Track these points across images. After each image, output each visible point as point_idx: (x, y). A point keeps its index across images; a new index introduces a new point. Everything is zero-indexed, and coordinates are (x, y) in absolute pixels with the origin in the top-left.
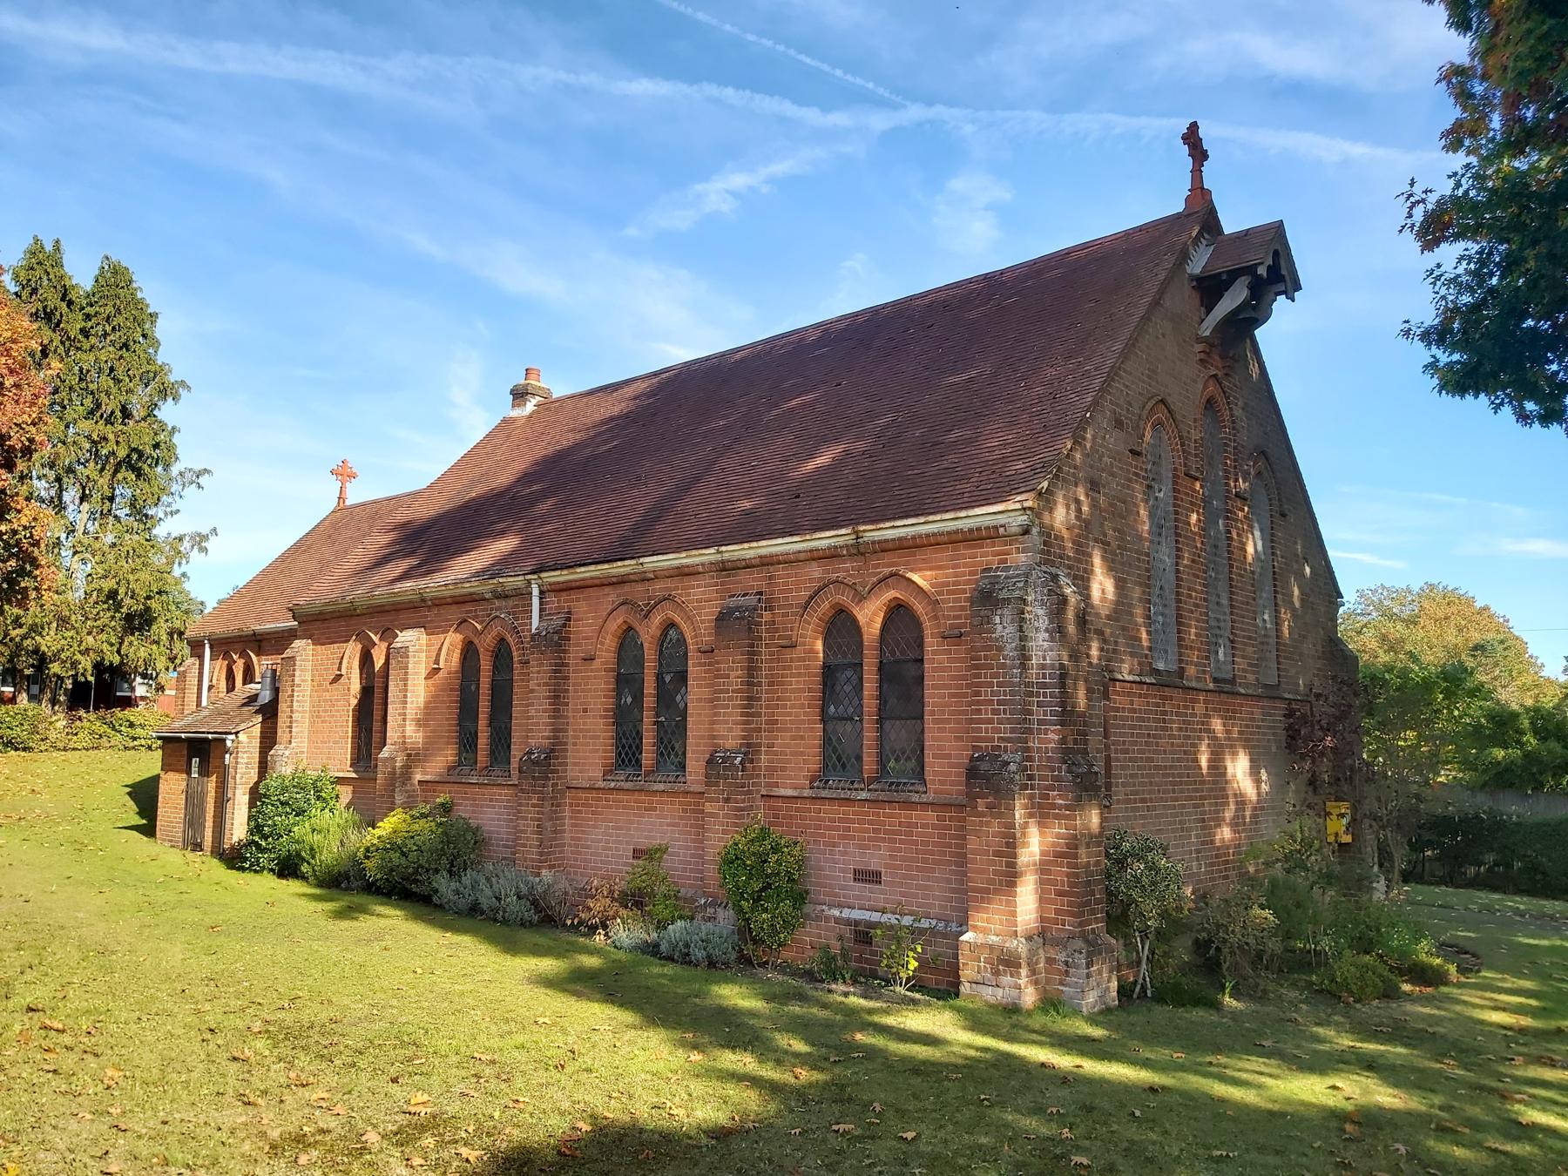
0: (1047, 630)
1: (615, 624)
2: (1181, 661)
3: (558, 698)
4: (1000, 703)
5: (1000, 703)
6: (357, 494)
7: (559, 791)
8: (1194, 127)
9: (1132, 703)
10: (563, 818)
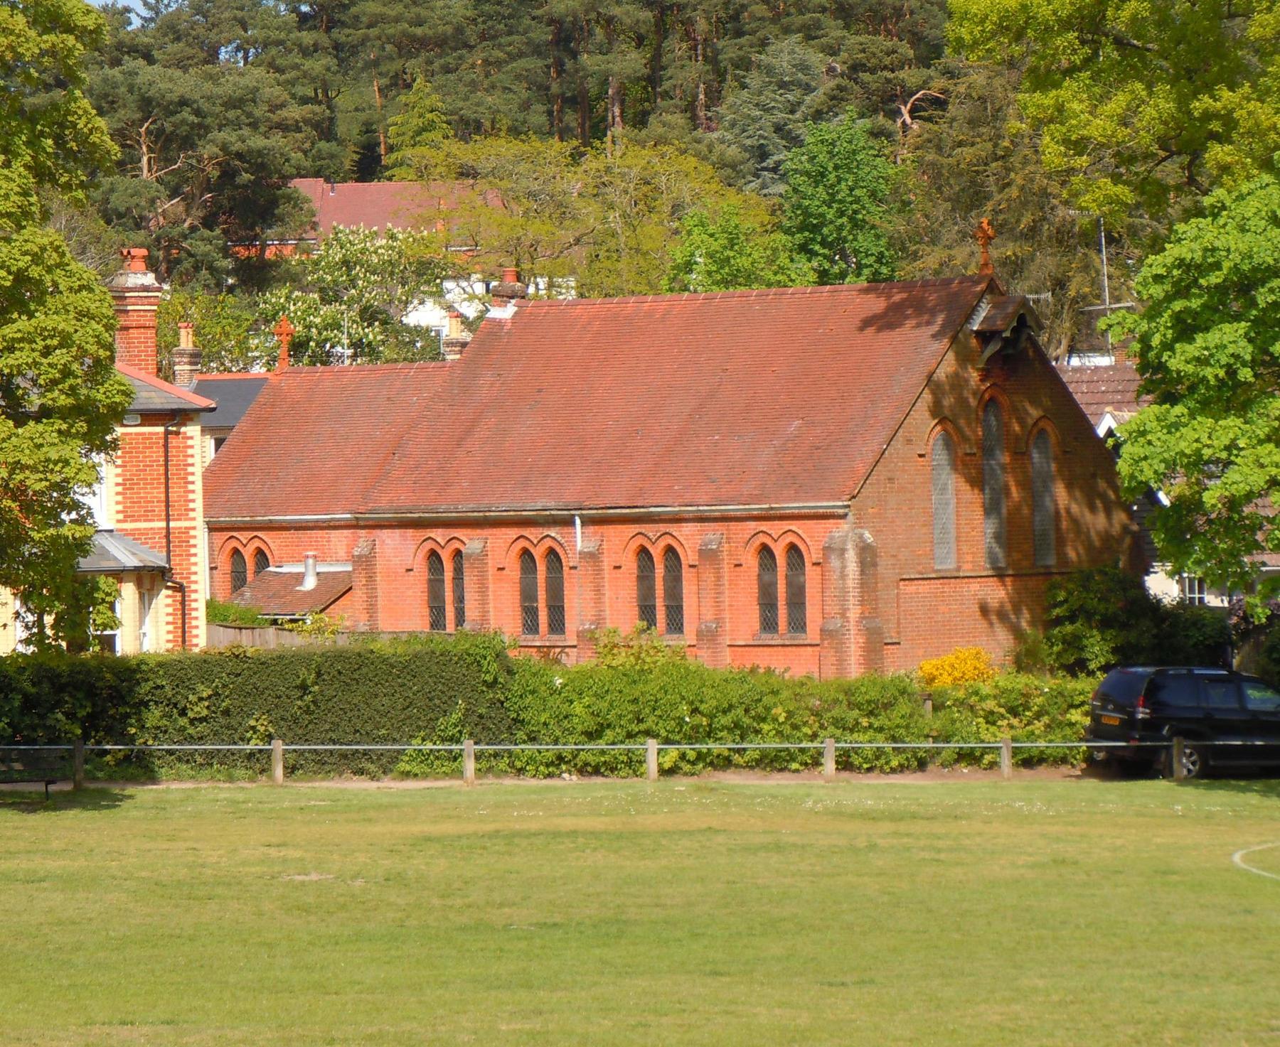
1: (634, 545)
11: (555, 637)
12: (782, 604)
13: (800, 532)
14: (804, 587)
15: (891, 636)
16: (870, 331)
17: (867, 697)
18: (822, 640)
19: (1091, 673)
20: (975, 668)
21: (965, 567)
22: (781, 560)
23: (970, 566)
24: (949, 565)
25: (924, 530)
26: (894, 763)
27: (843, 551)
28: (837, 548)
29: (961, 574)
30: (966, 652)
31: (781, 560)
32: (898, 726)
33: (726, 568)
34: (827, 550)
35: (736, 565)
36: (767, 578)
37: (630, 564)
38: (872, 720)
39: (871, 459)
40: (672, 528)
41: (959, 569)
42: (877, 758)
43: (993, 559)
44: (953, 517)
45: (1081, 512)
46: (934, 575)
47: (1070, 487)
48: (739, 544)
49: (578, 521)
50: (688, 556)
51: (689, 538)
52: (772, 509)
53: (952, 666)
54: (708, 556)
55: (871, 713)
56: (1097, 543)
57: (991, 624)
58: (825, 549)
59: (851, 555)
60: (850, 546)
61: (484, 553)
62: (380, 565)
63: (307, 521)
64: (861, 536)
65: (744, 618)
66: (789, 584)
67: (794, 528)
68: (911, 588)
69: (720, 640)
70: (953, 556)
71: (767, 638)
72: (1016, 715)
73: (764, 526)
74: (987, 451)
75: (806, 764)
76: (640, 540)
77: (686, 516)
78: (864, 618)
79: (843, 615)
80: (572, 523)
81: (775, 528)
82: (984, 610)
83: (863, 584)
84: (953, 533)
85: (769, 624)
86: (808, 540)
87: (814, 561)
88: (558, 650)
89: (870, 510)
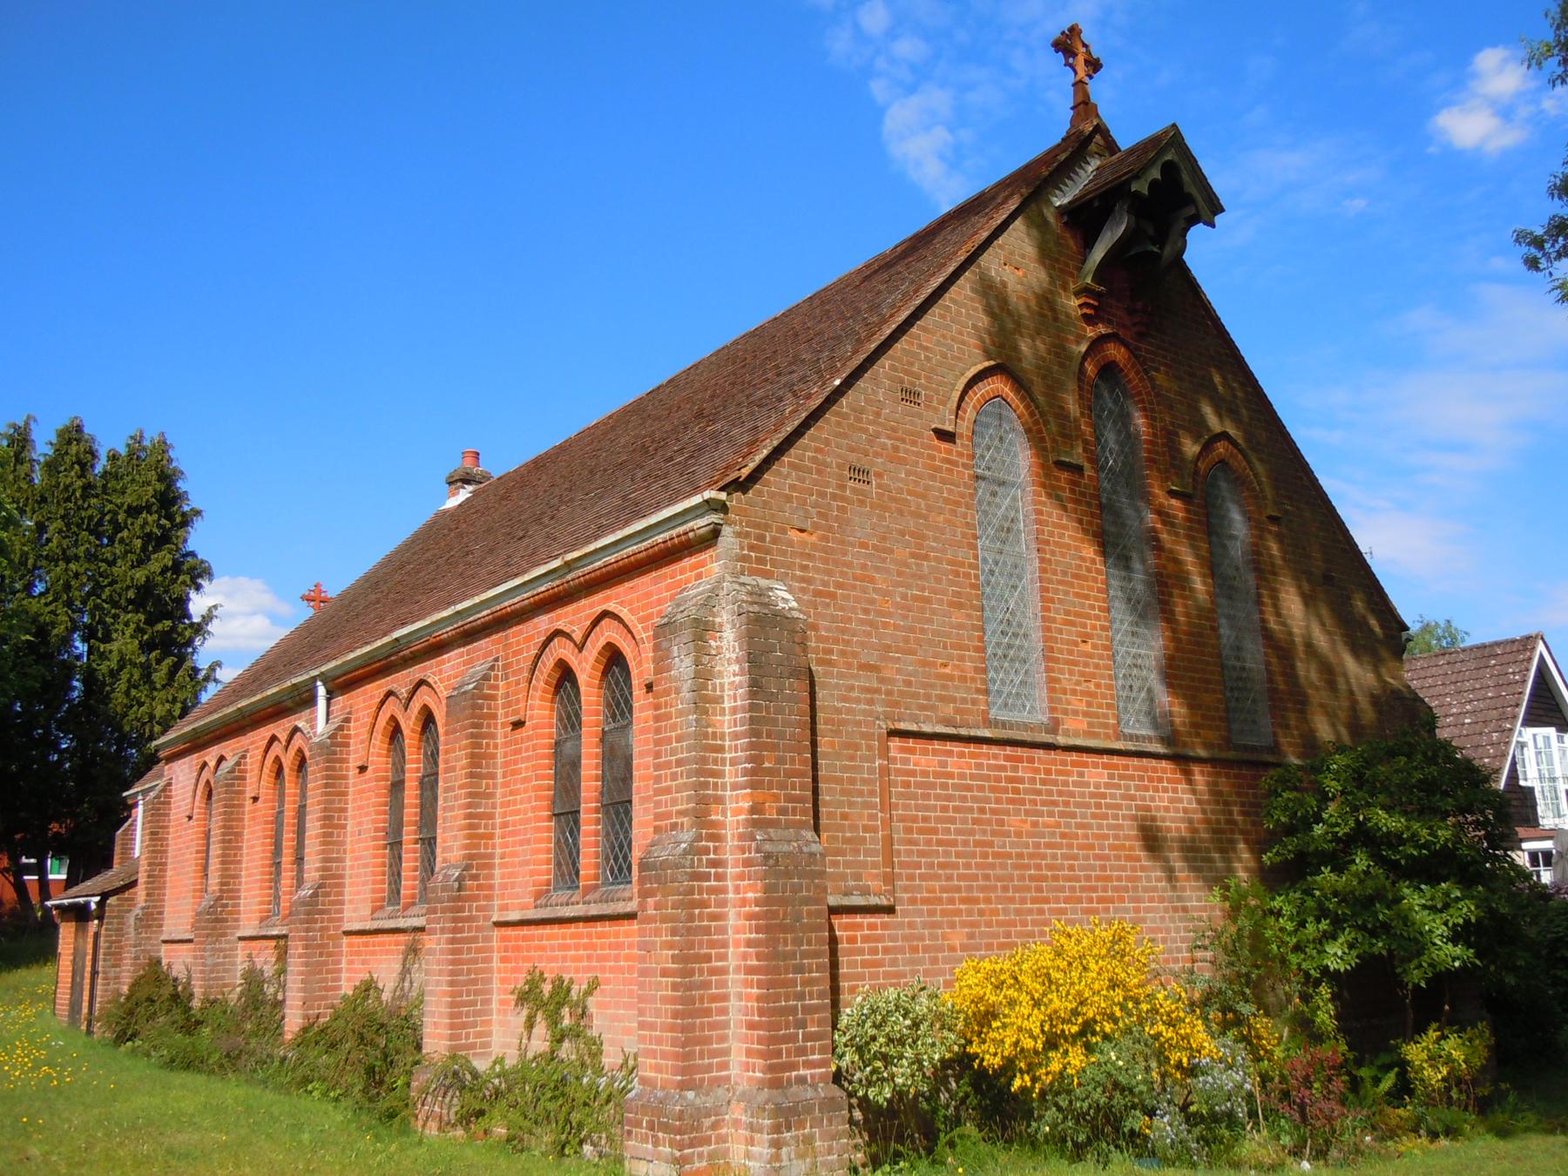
0: (738, 661)
2: (1053, 710)
4: (679, 763)
7: (329, 937)
9: (944, 764)
10: (339, 971)
20: (1113, 985)
21: (1069, 723)
23: (1082, 724)
24: (1032, 714)
25: (958, 617)
27: (702, 629)
29: (1061, 740)
30: (1087, 935)
34: (665, 631)
41: (1054, 727)
43: (1160, 722)
46: (987, 733)
47: (1308, 600)
49: (321, 691)
52: (569, 566)
54: (474, 705)
56: (1368, 714)
57: (1171, 877)
59: (728, 643)
60: (725, 617)
64: (759, 595)
68: (924, 759)
70: (1041, 694)
77: (446, 632)
82: (1151, 839)
84: (1036, 635)
89: (794, 535)
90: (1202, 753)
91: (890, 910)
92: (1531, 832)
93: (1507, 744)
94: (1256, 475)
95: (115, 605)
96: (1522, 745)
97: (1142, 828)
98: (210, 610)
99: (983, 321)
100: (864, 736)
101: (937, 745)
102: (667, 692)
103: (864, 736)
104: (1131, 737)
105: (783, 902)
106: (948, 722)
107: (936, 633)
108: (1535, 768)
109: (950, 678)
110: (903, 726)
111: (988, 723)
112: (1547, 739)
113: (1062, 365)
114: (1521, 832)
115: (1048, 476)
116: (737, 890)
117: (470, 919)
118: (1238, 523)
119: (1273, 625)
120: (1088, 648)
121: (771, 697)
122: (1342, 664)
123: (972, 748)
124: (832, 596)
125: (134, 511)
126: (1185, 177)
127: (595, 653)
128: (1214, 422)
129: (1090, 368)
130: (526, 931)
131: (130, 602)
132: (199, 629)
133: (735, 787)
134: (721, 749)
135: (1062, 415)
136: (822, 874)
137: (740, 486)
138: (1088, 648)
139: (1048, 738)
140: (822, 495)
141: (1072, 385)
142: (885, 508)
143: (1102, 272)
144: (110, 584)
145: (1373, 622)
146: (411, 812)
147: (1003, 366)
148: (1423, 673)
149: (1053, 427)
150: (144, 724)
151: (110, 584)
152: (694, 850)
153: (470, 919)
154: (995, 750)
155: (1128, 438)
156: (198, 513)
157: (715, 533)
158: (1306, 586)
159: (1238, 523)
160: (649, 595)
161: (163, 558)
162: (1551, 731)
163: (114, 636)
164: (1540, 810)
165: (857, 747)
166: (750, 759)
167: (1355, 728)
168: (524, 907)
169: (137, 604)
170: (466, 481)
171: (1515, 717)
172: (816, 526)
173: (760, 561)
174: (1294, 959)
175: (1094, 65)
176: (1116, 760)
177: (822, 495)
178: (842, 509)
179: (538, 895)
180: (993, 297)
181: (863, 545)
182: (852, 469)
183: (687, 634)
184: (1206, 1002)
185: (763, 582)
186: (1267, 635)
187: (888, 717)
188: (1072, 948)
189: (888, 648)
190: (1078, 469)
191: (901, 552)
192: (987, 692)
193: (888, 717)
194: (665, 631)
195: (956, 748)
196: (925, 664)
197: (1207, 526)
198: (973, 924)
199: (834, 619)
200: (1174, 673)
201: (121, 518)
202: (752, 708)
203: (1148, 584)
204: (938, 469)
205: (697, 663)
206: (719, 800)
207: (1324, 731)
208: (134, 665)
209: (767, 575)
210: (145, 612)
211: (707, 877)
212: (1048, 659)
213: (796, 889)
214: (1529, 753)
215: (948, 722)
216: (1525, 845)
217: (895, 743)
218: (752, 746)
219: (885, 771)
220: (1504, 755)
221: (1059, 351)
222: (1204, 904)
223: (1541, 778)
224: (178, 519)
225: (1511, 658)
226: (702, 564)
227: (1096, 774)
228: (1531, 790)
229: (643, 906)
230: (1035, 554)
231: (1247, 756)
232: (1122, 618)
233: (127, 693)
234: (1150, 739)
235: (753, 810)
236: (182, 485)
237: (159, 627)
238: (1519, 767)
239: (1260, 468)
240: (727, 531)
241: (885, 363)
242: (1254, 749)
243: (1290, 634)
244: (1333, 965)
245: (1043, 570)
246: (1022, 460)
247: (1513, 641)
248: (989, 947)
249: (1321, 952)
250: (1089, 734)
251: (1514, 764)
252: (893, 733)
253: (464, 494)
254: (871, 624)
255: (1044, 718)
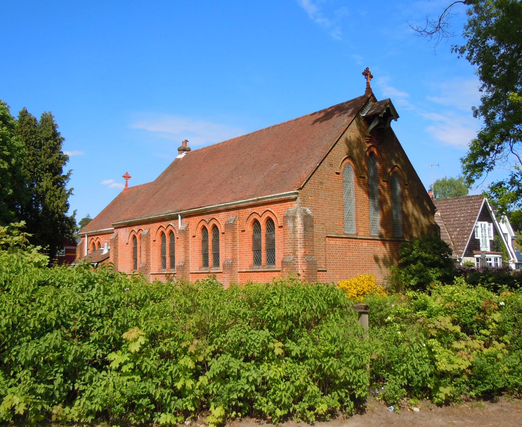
1: (200, 226)
3: (186, 248)
4: (290, 243)
5: (290, 243)
6: (132, 183)
8: (76, 210)
11: (172, 270)
12: (264, 251)
13: (272, 211)
14: (274, 240)
15: (322, 267)
16: (317, 124)
17: (281, 312)
18: (283, 267)
19: (53, 310)
20: (369, 286)
21: (360, 233)
22: (263, 227)
23: (362, 233)
24: (352, 232)
26: (322, 408)
27: (294, 218)
28: (290, 218)
29: (358, 237)
31: (263, 227)
32: (326, 354)
33: (238, 232)
34: (286, 217)
35: (243, 231)
36: (257, 237)
37: (199, 234)
38: (290, 345)
39: (311, 171)
40: (215, 216)
42: (298, 400)
44: (354, 207)
45: (419, 216)
46: (344, 236)
47: (413, 204)
48: (243, 221)
49: (180, 217)
50: (221, 229)
51: (222, 219)
52: (258, 200)
53: (356, 284)
54: (230, 227)
55: (289, 335)
56: (426, 230)
57: (380, 266)
58: (284, 217)
59: (299, 220)
60: (298, 215)
61: (148, 234)
62: (120, 242)
63: (110, 230)
64: (305, 210)
65: (246, 259)
66: (267, 239)
67: (269, 209)
68: (332, 242)
69: (234, 269)
70: (354, 229)
71: (256, 268)
72: (470, 333)
73: (255, 210)
74: (375, 179)
75: (186, 413)
76: (203, 223)
77: (221, 209)
78: (306, 255)
79: (294, 254)
80: (177, 218)
81: (260, 210)
82: (376, 259)
83: (305, 237)
84: (354, 215)
85: (257, 261)
86: (276, 215)
87: (280, 225)
88: (172, 275)
89: (310, 198)
90: (388, 239)
91: (326, 271)
92: (478, 252)
93: (472, 227)
94: (403, 175)
95: (42, 170)
96: (477, 227)
97: (374, 257)
98: (69, 171)
99: (346, 146)
100: (322, 237)
101: (335, 239)
102: (287, 229)
103: (322, 237)
104: (373, 236)
105: (310, 269)
106: (337, 234)
107: (335, 216)
108: (481, 233)
109: (337, 225)
110: (329, 235)
111: (345, 234)
112: (485, 225)
113: (362, 154)
114: (474, 252)
115: (358, 180)
116: (301, 267)
117: (234, 271)
118: (399, 188)
119: (405, 210)
120: (364, 217)
121: (307, 231)
122: (420, 218)
123: (341, 239)
124: (316, 209)
125: (47, 139)
126: (391, 111)
127: (265, 218)
128: (394, 164)
129: (368, 153)
130: (247, 273)
131: (47, 169)
132: (66, 177)
133: (300, 248)
134: (297, 241)
135: (361, 165)
136: (316, 264)
137: (301, 189)
138: (364, 217)
139: (356, 237)
140: (315, 189)
141: (364, 158)
142: (326, 190)
143: (371, 133)
144: (41, 163)
145: (428, 207)
146: (210, 247)
147: (350, 156)
148: (450, 204)
149: (360, 169)
150: (55, 209)
151: (41, 163)
152: (293, 260)
153: (234, 271)
154: (346, 239)
155: (376, 169)
156: (64, 139)
157: (296, 198)
158: (413, 200)
159: (399, 188)
160: (279, 208)
161: (57, 155)
162: (486, 223)
163: (43, 180)
164: (481, 246)
165: (320, 240)
166: (304, 243)
167: (422, 233)
168: (246, 269)
169: (50, 170)
170: (184, 150)
171: (475, 219)
172: (314, 195)
173: (304, 203)
174: (404, 282)
175: (371, 77)
176: (369, 241)
177: (315, 189)
178: (318, 191)
179: (250, 266)
180: (348, 143)
181: (322, 199)
182: (320, 183)
183: (291, 218)
184: (386, 290)
185: (305, 208)
186: (403, 212)
187: (326, 234)
188: (361, 279)
189: (326, 220)
190: (364, 178)
191: (329, 199)
192: (344, 228)
193: (326, 234)
194: (286, 217)
195: (338, 239)
196: (333, 222)
197: (392, 188)
198: (341, 274)
199: (317, 214)
200: (383, 224)
201: (42, 142)
202: (304, 233)
203: (378, 202)
204: (336, 181)
205: (294, 224)
206: (297, 250)
207: (415, 235)
208: (51, 190)
209: (305, 206)
210: (52, 173)
211: (295, 265)
212: (356, 220)
213: (312, 267)
214: (479, 229)
215: (337, 234)
216: (475, 256)
217: (327, 239)
218: (304, 241)
219: (325, 244)
220: (471, 230)
221: (361, 151)
222: (387, 271)
223: (482, 237)
224: (58, 142)
225: (476, 201)
226: (293, 204)
227: (365, 244)
228: (479, 240)
229: (282, 269)
230: (354, 197)
231: (397, 239)
232: (372, 210)
233: (50, 199)
234: (376, 236)
235: (304, 253)
236: (58, 130)
237: (56, 177)
238: (476, 233)
239: (404, 173)
240: (298, 198)
241: (327, 158)
242: (398, 238)
243: (408, 211)
244: (412, 284)
245: (356, 201)
246: (352, 176)
247: (478, 196)
248: (343, 279)
249: (410, 281)
250: (364, 236)
251: (474, 232)
252: (327, 237)
253: (183, 154)
254: (323, 215)
255: (355, 232)
